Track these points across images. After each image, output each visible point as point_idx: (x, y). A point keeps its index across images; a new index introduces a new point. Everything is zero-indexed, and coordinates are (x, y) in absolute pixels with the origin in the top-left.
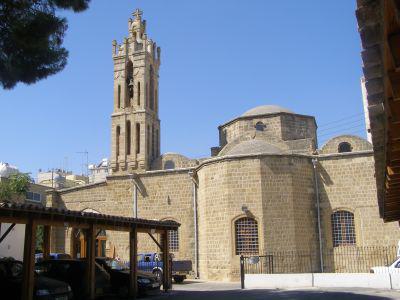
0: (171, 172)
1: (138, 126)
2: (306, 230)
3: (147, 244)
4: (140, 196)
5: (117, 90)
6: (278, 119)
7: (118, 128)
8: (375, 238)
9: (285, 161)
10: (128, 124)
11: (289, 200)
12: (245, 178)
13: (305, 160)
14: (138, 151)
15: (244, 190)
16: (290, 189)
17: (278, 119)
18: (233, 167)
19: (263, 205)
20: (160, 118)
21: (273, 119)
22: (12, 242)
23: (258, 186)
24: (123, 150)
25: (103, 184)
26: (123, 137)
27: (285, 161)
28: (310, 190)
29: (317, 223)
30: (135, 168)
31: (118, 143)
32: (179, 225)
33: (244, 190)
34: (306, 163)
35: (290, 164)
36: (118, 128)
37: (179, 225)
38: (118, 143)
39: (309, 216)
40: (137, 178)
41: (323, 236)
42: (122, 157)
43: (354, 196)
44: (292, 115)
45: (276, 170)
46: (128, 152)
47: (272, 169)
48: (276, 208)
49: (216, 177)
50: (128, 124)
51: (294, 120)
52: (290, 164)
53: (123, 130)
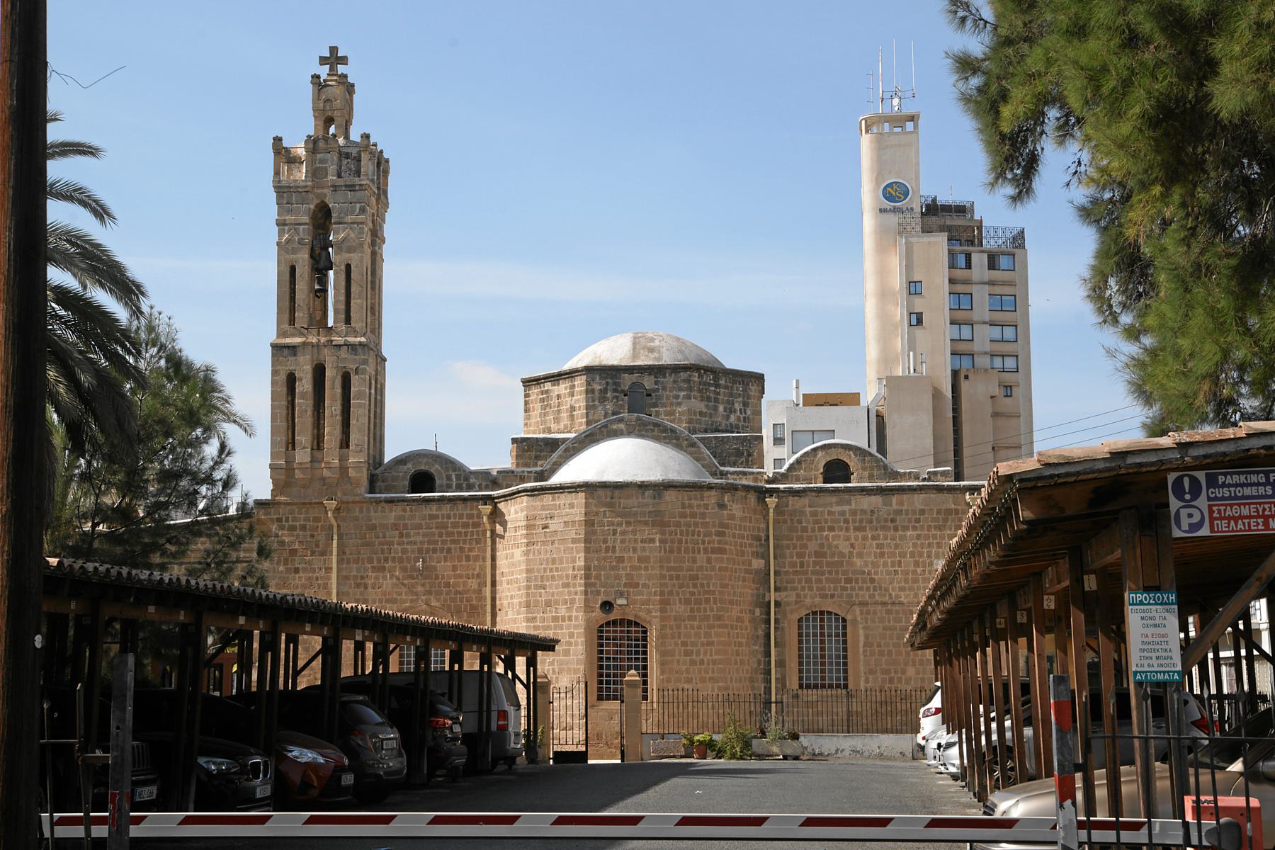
2: (745, 649)
3: (471, 662)
8: (887, 672)
10: (319, 371)
15: (621, 560)
20: (385, 353)
22: (1272, 766)
24: (304, 438)
26: (304, 404)
28: (758, 564)
29: (768, 636)
32: (557, 641)
33: (621, 560)
35: (722, 506)
37: (557, 641)
39: (753, 620)
41: (781, 664)
43: (848, 581)
48: (687, 602)
49: (555, 525)
50: (319, 371)
52: (722, 506)
53: (305, 385)
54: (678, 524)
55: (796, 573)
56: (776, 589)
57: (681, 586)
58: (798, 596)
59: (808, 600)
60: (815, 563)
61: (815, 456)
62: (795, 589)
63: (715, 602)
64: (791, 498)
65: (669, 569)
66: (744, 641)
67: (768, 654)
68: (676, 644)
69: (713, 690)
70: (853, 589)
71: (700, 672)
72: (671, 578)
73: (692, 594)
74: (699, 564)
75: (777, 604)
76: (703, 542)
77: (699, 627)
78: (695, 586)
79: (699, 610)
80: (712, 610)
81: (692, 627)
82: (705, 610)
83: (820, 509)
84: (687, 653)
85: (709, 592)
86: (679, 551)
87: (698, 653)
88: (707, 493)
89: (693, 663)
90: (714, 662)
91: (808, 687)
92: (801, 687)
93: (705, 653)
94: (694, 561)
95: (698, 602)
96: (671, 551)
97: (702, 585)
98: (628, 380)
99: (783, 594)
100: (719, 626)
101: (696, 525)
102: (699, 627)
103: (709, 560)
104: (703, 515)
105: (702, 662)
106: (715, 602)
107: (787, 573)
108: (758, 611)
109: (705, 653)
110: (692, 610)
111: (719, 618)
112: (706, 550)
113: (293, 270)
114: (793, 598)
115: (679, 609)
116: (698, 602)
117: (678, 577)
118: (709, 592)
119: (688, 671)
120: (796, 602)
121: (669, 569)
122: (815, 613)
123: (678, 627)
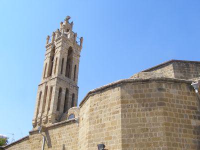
0: (68, 122)
1: (52, 88)
4: (46, 147)
5: (45, 65)
6: (171, 67)
7: (41, 93)
9: (154, 86)
11: (160, 134)
12: (105, 111)
13: (185, 86)
14: (49, 109)
15: (104, 125)
16: (161, 120)
17: (171, 67)
18: (95, 101)
19: (123, 141)
21: (166, 68)
23: (118, 117)
25: (27, 138)
26: (42, 99)
27: (154, 86)
30: (45, 123)
31: (40, 98)
34: (186, 90)
35: (160, 89)
36: (41, 93)
38: (40, 98)
40: (46, 130)
42: (39, 115)
44: (187, 63)
45: (148, 104)
46: (43, 111)
47: (135, 97)
51: (188, 67)
52: (160, 89)
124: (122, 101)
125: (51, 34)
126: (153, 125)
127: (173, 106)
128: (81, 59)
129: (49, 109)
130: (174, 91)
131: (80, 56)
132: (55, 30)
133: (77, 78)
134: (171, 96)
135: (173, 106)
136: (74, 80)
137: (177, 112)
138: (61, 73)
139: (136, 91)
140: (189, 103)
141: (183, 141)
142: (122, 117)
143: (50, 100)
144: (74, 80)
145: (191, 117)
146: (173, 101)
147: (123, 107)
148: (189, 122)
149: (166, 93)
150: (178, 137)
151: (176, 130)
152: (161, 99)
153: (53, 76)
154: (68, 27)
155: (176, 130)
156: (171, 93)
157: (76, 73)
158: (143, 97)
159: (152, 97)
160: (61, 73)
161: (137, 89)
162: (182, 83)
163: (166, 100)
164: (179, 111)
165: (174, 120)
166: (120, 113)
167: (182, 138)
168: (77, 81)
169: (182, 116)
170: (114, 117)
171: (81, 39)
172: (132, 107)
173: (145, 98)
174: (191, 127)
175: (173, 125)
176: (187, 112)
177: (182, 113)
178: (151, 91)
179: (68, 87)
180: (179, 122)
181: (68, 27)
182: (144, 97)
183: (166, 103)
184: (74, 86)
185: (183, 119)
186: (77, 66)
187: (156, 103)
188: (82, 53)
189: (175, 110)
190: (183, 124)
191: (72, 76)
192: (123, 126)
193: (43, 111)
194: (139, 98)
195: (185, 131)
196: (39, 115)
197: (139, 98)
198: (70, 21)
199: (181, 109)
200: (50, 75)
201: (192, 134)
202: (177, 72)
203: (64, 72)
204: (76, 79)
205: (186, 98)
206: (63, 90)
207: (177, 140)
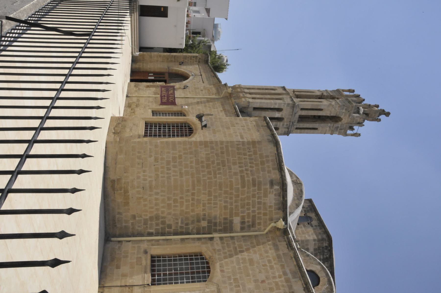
9: (275, 175)
14: (253, 98)
20: (291, 135)
23: (236, 138)
26: (267, 91)
35: (272, 183)
42: (246, 91)
46: (250, 94)
48: (208, 159)
54: (255, 153)
55: (235, 248)
56: (221, 238)
57: (217, 155)
58: (219, 250)
59: (217, 257)
60: (244, 260)
61: (317, 265)
62: (223, 248)
63: (209, 178)
64: (285, 243)
65: (227, 147)
66: (184, 208)
67: (176, 234)
68: (180, 151)
69: (150, 177)
70: (231, 284)
71: (162, 168)
72: (222, 148)
73: (213, 162)
74: (233, 167)
75: (211, 239)
76: (247, 170)
77: (192, 167)
78: (218, 164)
79: (203, 167)
80: (204, 176)
81: (191, 162)
82: (203, 171)
83: (283, 260)
84: (174, 159)
85: (215, 174)
86: (239, 154)
87: (174, 166)
88: (277, 172)
89: (168, 163)
90: (169, 178)
91: (153, 261)
92: (152, 257)
93: (175, 171)
94: (234, 164)
95: (208, 166)
96: (238, 149)
97: (219, 169)
98: (313, 215)
99: (219, 242)
100: (193, 182)
101: (257, 165)
102: (192, 167)
103: (236, 174)
104: (263, 170)
105: (169, 169)
106: (209, 178)
107: (234, 243)
108: (204, 224)
109: (175, 171)
110: (202, 162)
111: (199, 181)
112: (242, 171)
113: (313, 92)
114: (217, 248)
115: (203, 153)
116: (208, 166)
117: (222, 153)
118: (215, 174)
119: (162, 159)
120: (214, 250)
121: (227, 147)
122: (207, 263)
123: (191, 153)
124: (303, 241)
125: (356, 93)
126: (229, 172)
127: (254, 196)
128: (328, 136)
129: (253, 98)
130: (271, 199)
131: (332, 134)
132: (362, 96)
133: (301, 133)
134: (266, 196)
135: (254, 196)
136: (297, 128)
137: (246, 201)
138: (302, 109)
139: (267, 156)
140: (260, 218)
141: (215, 204)
142: (237, 141)
143: (265, 99)
144: (297, 128)
145: (243, 217)
146: (259, 198)
147: (248, 143)
148: (237, 215)
149: (269, 190)
150: (219, 199)
151: (226, 197)
152: (260, 183)
153: (296, 100)
154: (374, 114)
155: (226, 197)
156: (269, 195)
157: (306, 131)
158: (261, 163)
159: (261, 173)
160: (302, 109)
161: (270, 158)
162: (283, 211)
163: (259, 189)
164: (248, 204)
165: (237, 196)
166: (241, 140)
167: (219, 203)
168: (297, 133)
169: (243, 207)
170: (237, 136)
171: (357, 135)
172: (249, 152)
173: (260, 166)
174: (231, 216)
175: (231, 194)
176: (249, 214)
177: (246, 207)
178: (269, 172)
179: (285, 119)
180: (236, 202)
181: (374, 114)
182: (253, 148)
183: (256, 188)
184: (288, 128)
185: (240, 207)
186: (316, 131)
187: (255, 177)
188: (337, 138)
189: (248, 198)
190: (234, 207)
191: (302, 125)
192: (227, 142)
193: (250, 94)
194: (260, 160)
195: (226, 208)
196: (246, 91)
197: (260, 160)
198: (382, 117)
199: (251, 206)
200: (297, 97)
201: (223, 216)
202: (315, 244)
203: (304, 113)
204: (299, 131)
205: (265, 214)
206: (281, 113)
207: (216, 197)
